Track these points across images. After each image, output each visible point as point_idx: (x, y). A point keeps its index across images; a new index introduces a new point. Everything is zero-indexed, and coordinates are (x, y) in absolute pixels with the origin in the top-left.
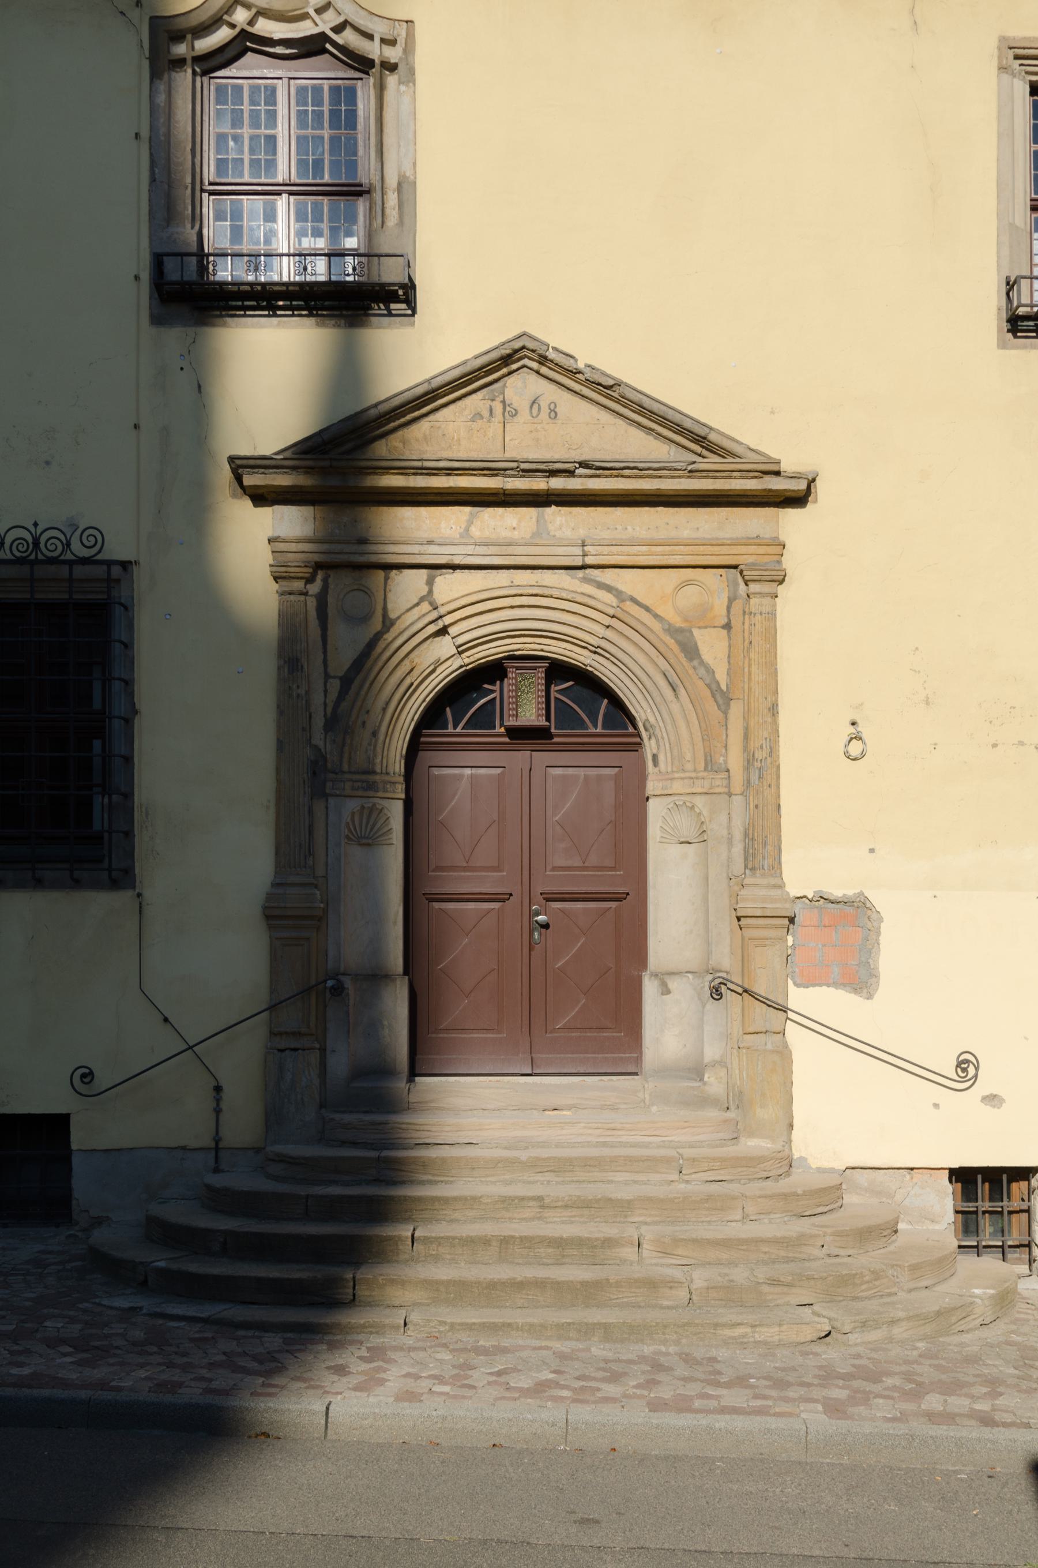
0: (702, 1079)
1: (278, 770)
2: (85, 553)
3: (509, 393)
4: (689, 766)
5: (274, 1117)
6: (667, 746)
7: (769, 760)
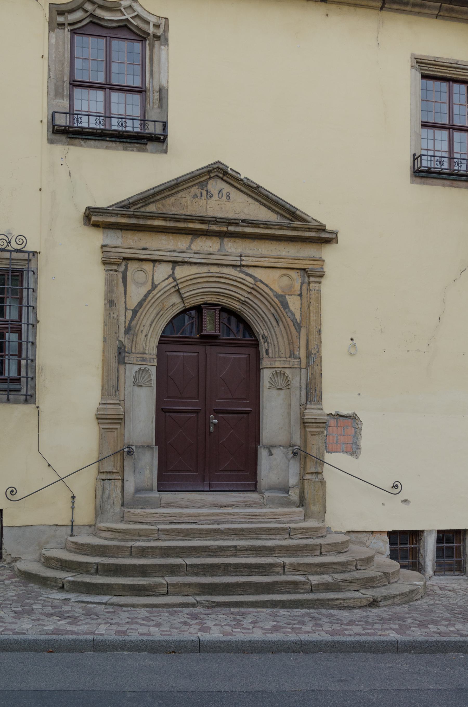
0: (288, 493)
1: (104, 352)
2: (19, 247)
3: (209, 187)
4: (283, 355)
5: (99, 511)
6: (273, 346)
7: (318, 354)
